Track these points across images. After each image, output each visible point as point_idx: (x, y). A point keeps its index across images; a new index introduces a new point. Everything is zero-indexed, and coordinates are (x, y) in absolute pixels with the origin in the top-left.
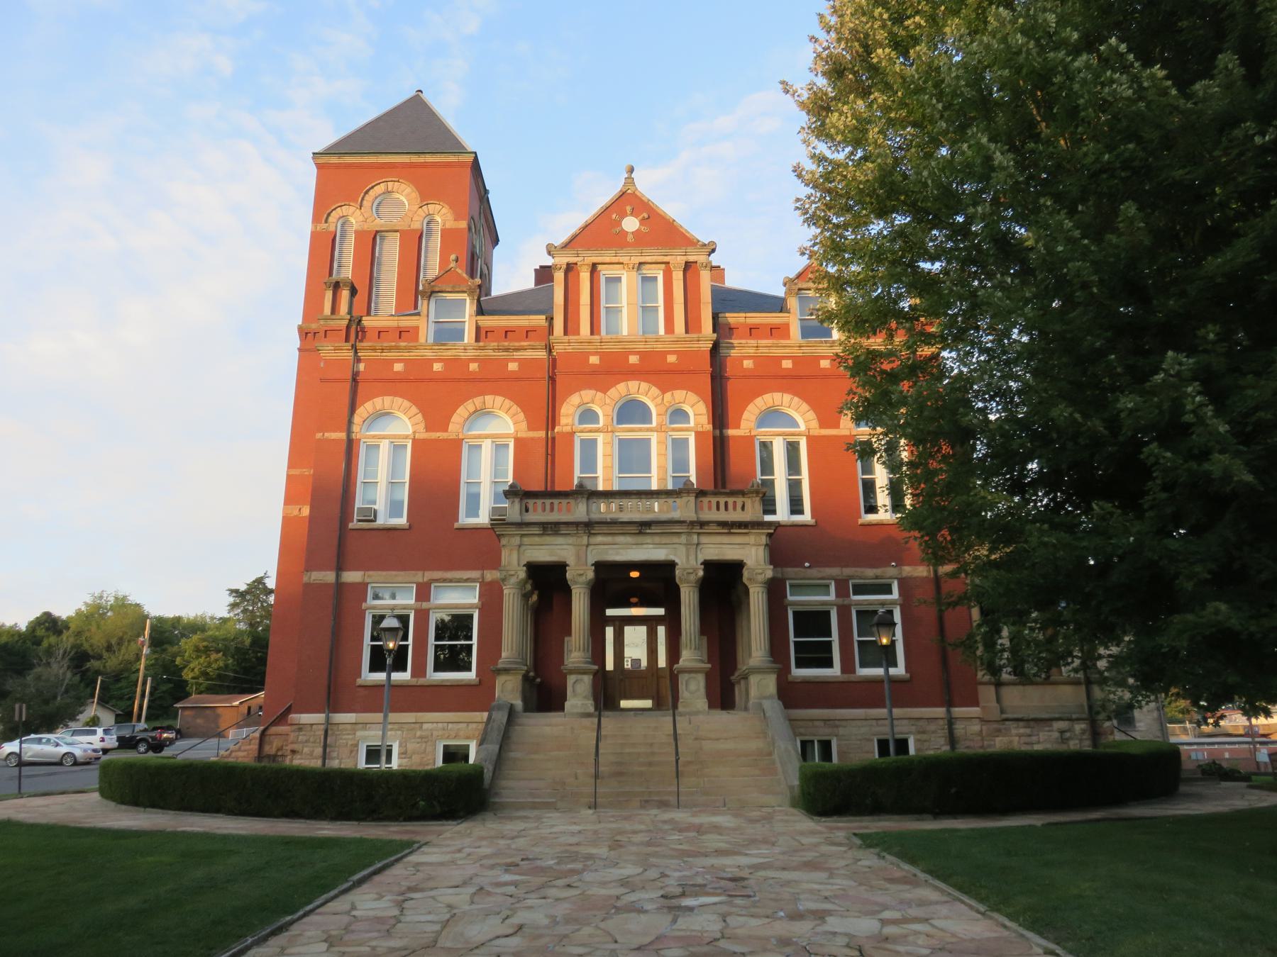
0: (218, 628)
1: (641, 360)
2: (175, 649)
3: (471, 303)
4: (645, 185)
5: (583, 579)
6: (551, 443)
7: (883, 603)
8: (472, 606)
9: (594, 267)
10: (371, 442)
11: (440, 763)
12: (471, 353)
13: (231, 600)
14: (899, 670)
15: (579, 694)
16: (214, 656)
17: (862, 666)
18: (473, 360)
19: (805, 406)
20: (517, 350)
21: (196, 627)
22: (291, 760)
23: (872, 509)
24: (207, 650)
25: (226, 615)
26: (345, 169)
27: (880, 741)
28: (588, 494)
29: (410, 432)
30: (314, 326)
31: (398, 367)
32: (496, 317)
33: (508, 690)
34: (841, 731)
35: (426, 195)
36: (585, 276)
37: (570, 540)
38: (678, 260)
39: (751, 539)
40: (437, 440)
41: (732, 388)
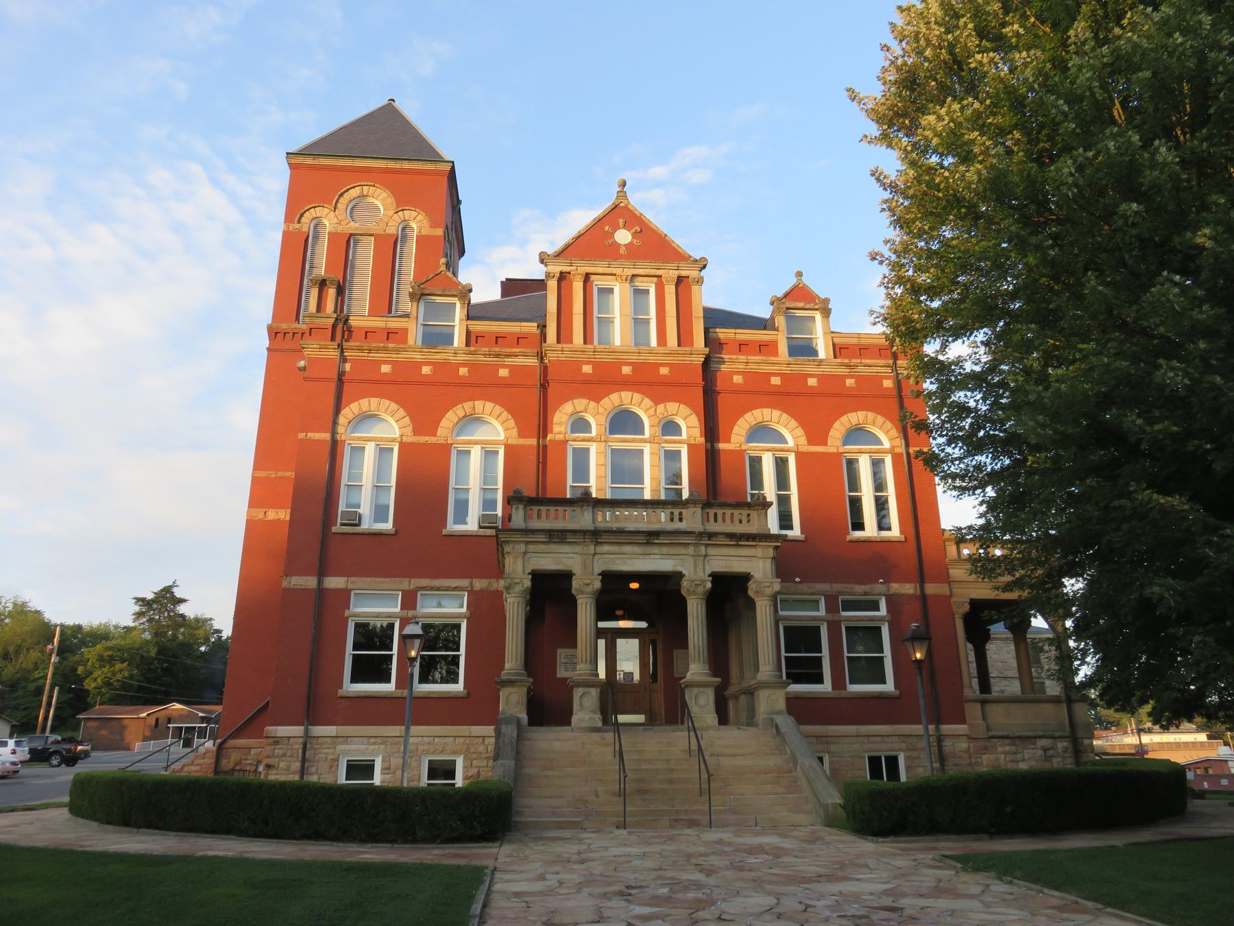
0: (123, 638)
1: (633, 371)
2: (77, 658)
3: (462, 308)
4: (636, 200)
5: (589, 589)
6: (542, 451)
7: (872, 619)
8: (460, 616)
9: (587, 277)
10: (356, 444)
11: (424, 781)
12: (461, 358)
13: (137, 608)
14: (889, 686)
15: (585, 709)
16: (118, 666)
17: (851, 683)
18: (464, 365)
19: (794, 423)
20: (508, 356)
21: (98, 636)
22: (267, 775)
23: (859, 526)
24: (111, 660)
25: (132, 624)
26: (320, 169)
27: (870, 759)
28: (585, 500)
29: (397, 435)
30: (284, 326)
31: (386, 369)
32: (487, 323)
33: (512, 702)
34: (833, 748)
35: (402, 201)
36: (578, 286)
37: (578, 549)
38: (670, 273)
39: (759, 552)
40: (425, 445)
41: (723, 402)
